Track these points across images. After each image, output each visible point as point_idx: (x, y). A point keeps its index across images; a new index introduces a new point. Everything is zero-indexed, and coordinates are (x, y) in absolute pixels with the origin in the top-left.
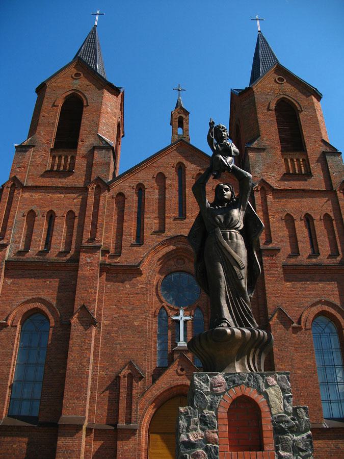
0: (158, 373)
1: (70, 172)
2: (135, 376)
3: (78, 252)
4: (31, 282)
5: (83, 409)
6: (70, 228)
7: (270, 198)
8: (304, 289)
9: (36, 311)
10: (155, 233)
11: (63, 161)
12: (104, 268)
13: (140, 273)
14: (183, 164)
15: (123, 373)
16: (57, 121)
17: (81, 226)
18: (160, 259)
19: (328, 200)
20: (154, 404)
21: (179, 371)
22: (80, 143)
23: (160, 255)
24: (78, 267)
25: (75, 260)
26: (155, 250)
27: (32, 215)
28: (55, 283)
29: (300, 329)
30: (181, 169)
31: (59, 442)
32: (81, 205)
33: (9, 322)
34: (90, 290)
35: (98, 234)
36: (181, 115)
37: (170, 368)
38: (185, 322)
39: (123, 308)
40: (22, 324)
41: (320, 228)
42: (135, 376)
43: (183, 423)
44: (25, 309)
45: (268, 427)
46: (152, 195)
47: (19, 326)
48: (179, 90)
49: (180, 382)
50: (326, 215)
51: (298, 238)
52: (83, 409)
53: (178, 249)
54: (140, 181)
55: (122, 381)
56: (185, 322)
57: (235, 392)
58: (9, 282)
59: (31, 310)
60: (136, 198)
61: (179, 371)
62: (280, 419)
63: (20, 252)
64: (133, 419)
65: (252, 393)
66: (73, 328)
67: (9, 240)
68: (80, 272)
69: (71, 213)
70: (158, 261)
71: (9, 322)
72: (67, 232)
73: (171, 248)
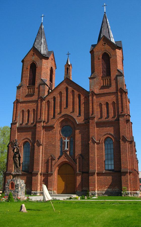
1: (33, 95)
2: (53, 159)
3: (36, 123)
4: (24, 133)
6: (34, 114)
7: (95, 97)
8: (102, 130)
9: (27, 142)
10: (58, 114)
11: (31, 90)
12: (44, 127)
13: (54, 128)
15: (49, 158)
16: (29, 75)
17: (37, 114)
18: (60, 123)
19: (115, 96)
22: (36, 83)
23: (60, 121)
24: (36, 127)
25: (35, 125)
28: (31, 133)
29: (100, 143)
30: (67, 89)
31: (33, 178)
33: (20, 146)
34: (40, 135)
35: (42, 116)
36: (67, 67)
38: (67, 142)
40: (23, 146)
41: (111, 107)
43: (6, 185)
44: (24, 141)
45: (14, 186)
46: (58, 100)
47: (22, 146)
48: (68, 54)
49: (65, 160)
50: (114, 102)
51: (103, 112)
54: (54, 96)
57: (11, 182)
58: (19, 134)
59: (25, 142)
60: (53, 102)
62: (16, 185)
63: (21, 124)
64: (52, 171)
65: (13, 182)
66: (35, 147)
67: (17, 121)
68: (37, 129)
69: (34, 109)
71: (20, 146)
72: (33, 116)
73: (63, 119)
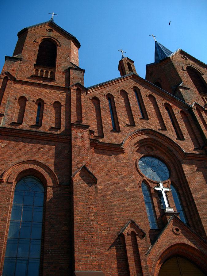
0: (155, 235)
5: (97, 263)
14: (137, 88)
18: (135, 144)
20: (160, 260)
21: (175, 231)
25: (68, 133)
26: (132, 137)
27: (23, 100)
32: (66, 99)
37: (167, 227)
39: (114, 176)
42: (137, 234)
46: (120, 102)
49: (178, 241)
52: (97, 263)
53: (150, 138)
55: (126, 239)
56: (166, 192)
61: (175, 231)
66: (75, 185)
70: (135, 145)
